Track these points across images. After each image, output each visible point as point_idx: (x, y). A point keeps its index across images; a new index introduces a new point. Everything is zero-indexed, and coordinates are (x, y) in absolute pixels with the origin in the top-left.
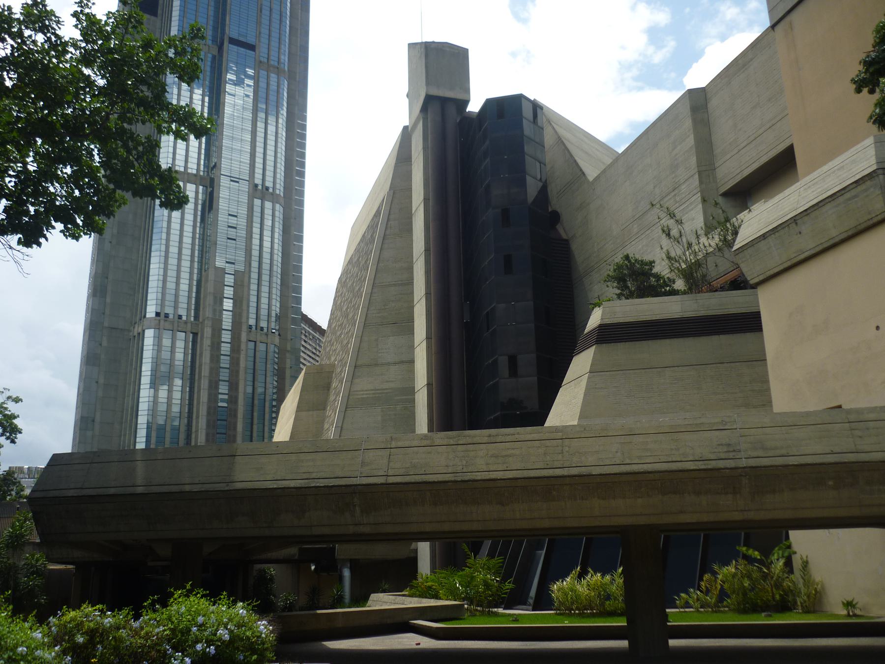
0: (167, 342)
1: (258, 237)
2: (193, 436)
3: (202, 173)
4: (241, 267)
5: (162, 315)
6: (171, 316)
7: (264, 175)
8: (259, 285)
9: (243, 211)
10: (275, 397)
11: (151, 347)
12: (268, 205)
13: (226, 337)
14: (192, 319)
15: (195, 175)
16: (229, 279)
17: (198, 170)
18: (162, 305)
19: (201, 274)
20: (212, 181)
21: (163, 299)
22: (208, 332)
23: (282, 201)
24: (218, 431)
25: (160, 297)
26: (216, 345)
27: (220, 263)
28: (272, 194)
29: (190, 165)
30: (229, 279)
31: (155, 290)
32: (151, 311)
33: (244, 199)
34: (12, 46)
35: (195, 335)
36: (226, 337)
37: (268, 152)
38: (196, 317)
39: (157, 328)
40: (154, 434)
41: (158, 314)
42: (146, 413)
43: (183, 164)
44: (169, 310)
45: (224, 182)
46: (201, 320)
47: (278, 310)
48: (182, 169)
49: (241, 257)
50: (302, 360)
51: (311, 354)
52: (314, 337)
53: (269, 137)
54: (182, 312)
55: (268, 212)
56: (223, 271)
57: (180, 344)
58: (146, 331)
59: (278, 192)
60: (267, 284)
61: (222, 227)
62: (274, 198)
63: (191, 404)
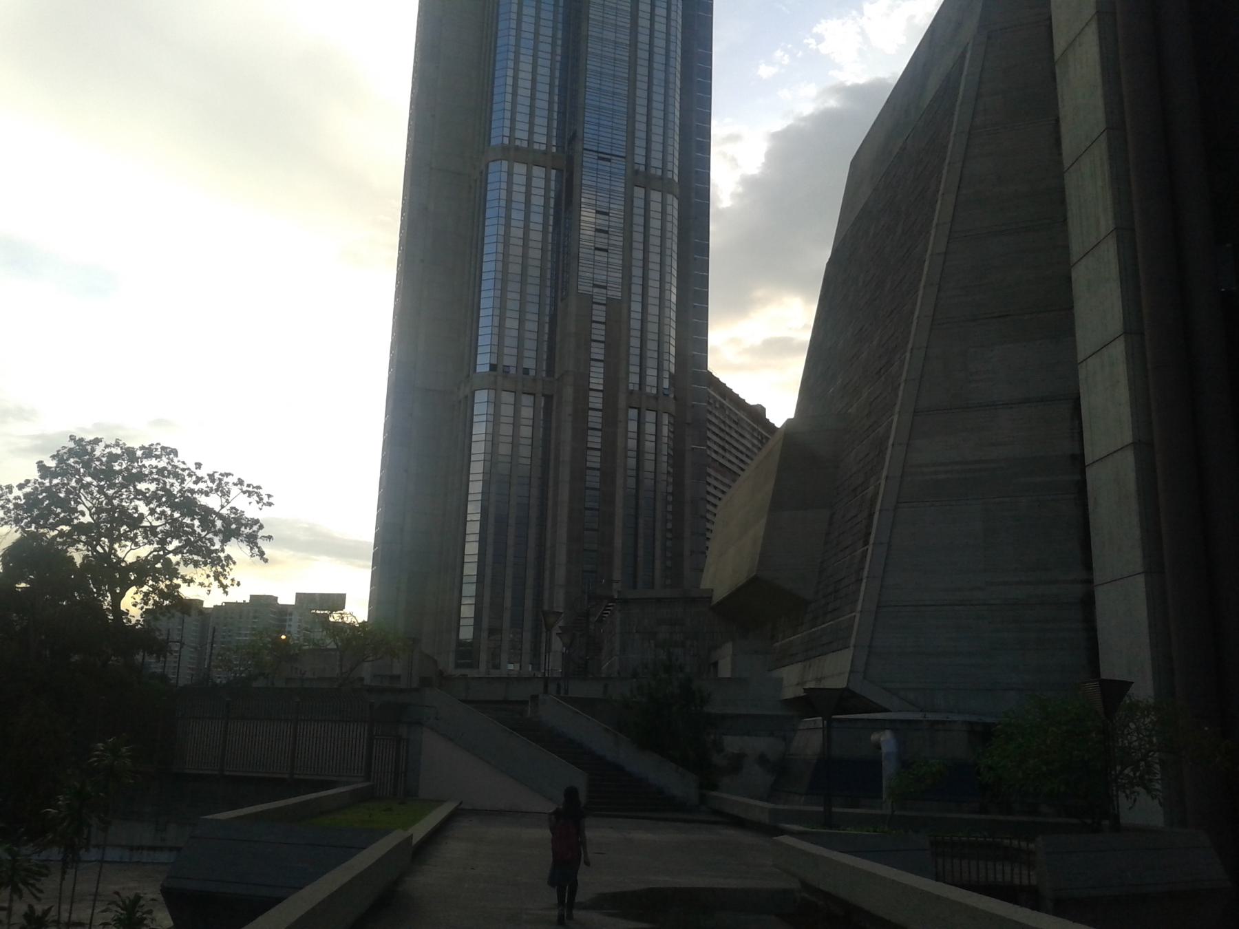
0: (507, 410)
1: (644, 119)
2: (546, 595)
3: (554, 149)
4: (616, 293)
5: (500, 368)
6: (513, 371)
7: (648, 149)
8: (646, 251)
9: (617, 207)
10: (670, 489)
11: (490, 312)
12: (656, 196)
13: (596, 400)
14: (544, 374)
15: (545, 153)
16: (599, 313)
17: (548, 145)
18: (500, 355)
19: (556, 305)
20: (570, 160)
21: (500, 345)
22: (569, 392)
23: (677, 191)
24: (588, 505)
25: (495, 342)
26: (581, 410)
27: (585, 287)
28: (661, 178)
29: (536, 138)
30: (599, 313)
31: (489, 330)
32: (483, 362)
33: (620, 187)
34: (226, 578)
35: (549, 398)
36: (596, 400)
37: (655, 113)
38: (550, 371)
39: (493, 387)
40: (488, 571)
41: (493, 367)
42: (482, 457)
43: (525, 136)
44: (510, 361)
45: (589, 160)
46: (557, 376)
47: (673, 370)
48: (525, 144)
49: (616, 276)
50: (709, 434)
51: (717, 431)
52: (722, 406)
53: (655, 89)
54: (530, 364)
55: (656, 207)
56: (590, 300)
57: (527, 412)
58: (491, 164)
59: (669, 175)
60: (661, 123)
61: (587, 231)
62: (663, 184)
63: (547, 429)
